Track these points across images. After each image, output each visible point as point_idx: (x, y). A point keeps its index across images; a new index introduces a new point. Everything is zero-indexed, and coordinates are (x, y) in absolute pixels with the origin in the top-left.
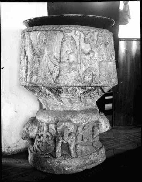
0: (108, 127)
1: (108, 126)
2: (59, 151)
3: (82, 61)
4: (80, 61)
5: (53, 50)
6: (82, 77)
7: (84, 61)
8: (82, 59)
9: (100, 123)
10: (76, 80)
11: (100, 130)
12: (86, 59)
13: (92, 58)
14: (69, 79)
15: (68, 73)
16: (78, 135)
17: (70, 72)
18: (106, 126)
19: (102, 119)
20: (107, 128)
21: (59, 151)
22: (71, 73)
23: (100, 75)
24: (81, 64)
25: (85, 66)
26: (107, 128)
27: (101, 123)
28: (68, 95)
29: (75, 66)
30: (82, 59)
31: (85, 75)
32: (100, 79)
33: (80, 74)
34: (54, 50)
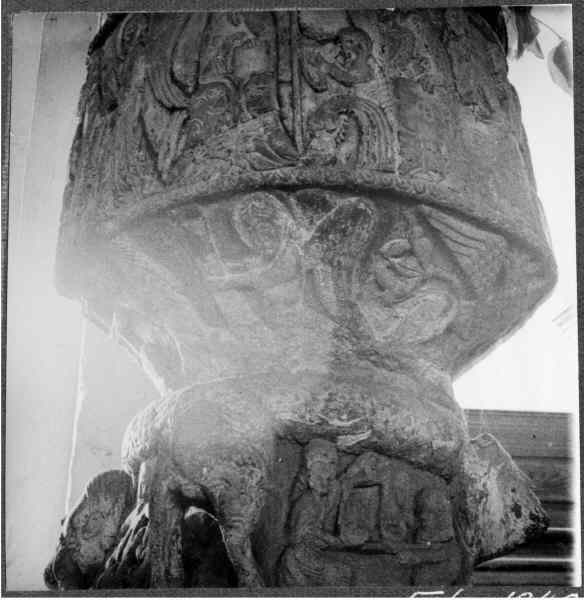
0: (525, 512)
1: (522, 503)
2: (167, 572)
3: (301, 67)
4: (292, 72)
5: (169, 52)
6: (298, 138)
7: (312, 71)
8: (300, 61)
9: (473, 481)
10: (265, 153)
11: (477, 529)
12: (319, 61)
13: (354, 56)
14: (229, 151)
15: (228, 124)
16: (297, 500)
17: (235, 121)
18: (510, 503)
19: (486, 463)
20: (518, 515)
21: (167, 572)
22: (240, 125)
23: (399, 133)
24: (296, 82)
25: (316, 91)
26: (518, 515)
27: (479, 486)
28: (246, 269)
29: (262, 89)
30: (300, 61)
31: (315, 126)
32: (401, 153)
33: (290, 128)
34: (174, 51)
